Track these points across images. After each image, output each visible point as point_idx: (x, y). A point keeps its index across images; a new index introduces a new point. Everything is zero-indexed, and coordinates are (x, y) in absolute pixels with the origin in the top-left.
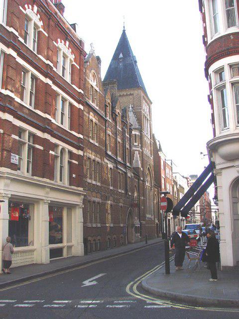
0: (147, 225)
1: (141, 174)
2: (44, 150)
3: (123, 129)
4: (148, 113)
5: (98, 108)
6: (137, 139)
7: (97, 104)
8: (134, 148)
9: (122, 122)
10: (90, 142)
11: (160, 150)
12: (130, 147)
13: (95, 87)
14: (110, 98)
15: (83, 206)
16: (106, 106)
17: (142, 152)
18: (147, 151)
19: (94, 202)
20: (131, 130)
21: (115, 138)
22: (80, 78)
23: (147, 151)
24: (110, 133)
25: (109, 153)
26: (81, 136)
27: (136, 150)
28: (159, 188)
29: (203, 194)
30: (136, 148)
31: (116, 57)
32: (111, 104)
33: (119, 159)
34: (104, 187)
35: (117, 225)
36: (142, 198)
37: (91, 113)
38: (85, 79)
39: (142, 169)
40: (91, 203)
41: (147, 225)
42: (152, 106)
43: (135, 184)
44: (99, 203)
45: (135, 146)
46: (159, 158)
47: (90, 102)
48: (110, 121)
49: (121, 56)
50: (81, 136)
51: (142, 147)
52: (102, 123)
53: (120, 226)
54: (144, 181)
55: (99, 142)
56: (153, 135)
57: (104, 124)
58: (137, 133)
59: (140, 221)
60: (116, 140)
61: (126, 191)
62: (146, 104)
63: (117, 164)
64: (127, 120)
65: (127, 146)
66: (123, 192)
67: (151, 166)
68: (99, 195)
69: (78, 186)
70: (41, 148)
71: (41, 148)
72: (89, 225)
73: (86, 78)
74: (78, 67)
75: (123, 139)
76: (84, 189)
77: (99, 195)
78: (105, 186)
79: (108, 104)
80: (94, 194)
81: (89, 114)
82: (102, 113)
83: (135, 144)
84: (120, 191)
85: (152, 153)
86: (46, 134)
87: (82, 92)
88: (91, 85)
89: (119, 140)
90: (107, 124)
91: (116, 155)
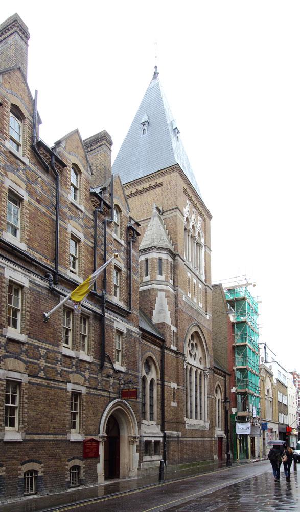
17: (176, 297)
21: (54, 217)
27: (161, 290)
36: (174, 385)
39: (174, 328)
51: (174, 286)
58: (165, 256)
59: (163, 430)
83: (162, 278)
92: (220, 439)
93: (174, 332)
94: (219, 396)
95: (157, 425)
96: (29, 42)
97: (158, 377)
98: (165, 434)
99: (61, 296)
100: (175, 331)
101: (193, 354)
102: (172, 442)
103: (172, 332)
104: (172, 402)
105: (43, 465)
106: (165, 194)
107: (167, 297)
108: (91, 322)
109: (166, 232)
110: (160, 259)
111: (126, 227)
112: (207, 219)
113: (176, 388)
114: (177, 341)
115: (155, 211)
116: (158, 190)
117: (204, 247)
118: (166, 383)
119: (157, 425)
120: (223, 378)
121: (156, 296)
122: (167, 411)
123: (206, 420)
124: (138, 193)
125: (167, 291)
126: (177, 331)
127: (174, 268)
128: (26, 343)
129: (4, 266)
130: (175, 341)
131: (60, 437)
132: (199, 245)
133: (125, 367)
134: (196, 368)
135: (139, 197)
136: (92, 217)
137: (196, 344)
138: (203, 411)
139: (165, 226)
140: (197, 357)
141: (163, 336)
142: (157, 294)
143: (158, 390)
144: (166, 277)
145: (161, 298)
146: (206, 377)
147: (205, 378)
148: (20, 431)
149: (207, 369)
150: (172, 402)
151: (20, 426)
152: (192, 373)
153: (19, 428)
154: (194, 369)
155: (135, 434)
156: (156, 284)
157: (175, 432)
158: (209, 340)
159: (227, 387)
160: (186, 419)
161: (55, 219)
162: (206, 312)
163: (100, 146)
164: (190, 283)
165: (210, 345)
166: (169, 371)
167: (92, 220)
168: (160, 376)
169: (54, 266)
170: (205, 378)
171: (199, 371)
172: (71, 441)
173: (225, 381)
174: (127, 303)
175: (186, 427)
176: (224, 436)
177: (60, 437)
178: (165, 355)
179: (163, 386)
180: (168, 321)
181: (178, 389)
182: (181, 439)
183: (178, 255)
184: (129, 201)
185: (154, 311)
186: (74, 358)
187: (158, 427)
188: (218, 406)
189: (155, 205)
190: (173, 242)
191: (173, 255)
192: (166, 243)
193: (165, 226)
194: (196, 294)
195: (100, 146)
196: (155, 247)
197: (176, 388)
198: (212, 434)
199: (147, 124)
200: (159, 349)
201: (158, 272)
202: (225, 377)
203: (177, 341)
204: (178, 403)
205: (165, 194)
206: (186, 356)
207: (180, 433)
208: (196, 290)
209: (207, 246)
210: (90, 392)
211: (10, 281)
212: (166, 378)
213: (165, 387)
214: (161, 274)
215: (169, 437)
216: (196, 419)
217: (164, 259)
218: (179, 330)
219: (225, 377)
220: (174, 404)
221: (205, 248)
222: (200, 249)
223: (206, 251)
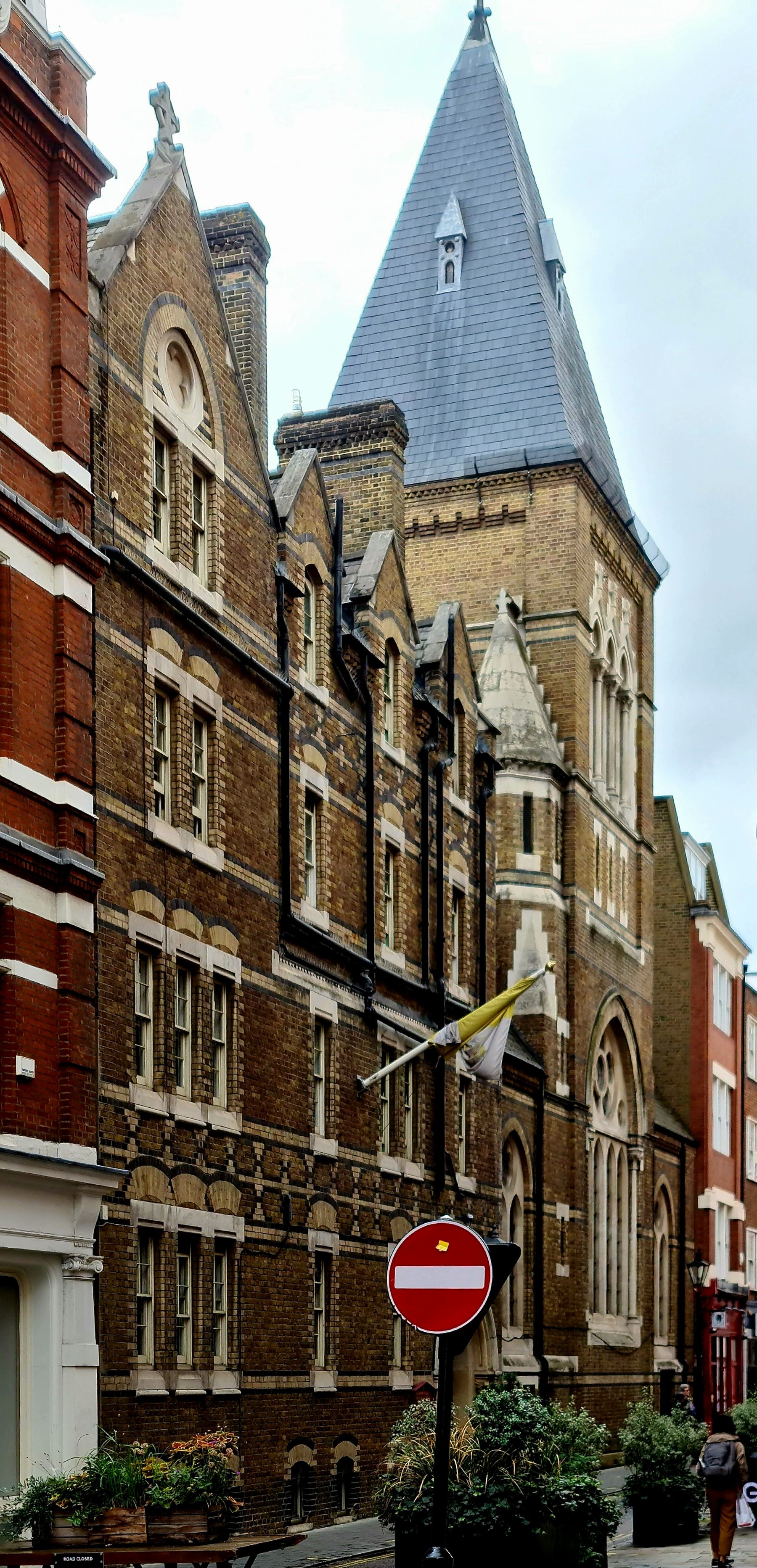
0: (589, 1380)
1: (554, 1062)
2: (62, 990)
3: (422, 757)
4: (624, 648)
5: (215, 601)
6: (539, 825)
7: (212, 576)
8: (519, 893)
9: (419, 708)
10: (159, 844)
11: (714, 903)
12: (480, 879)
13: (189, 438)
14: (324, 534)
15: (98, 1266)
16: (286, 591)
17: (569, 919)
18: (609, 910)
19: (189, 1240)
20: (486, 768)
21: (363, 815)
22: (57, 369)
23: (609, 910)
24: (322, 786)
25: (311, 912)
26: (82, 800)
27: (529, 905)
28: (690, 1154)
29: (281, 878)
30: (527, 886)
31: (414, 243)
32: (324, 573)
33: (392, 958)
34: (269, 1145)
35: (364, 1381)
36: (563, 1211)
37: (161, 637)
38: (104, 376)
39: (563, 1027)
40: (169, 1245)
41: (589, 1380)
42: (663, 602)
43: (513, 1123)
44: (224, 1244)
45: (526, 878)
46: (701, 957)
47: (156, 553)
48: (323, 695)
49: (451, 223)
50: (82, 800)
51: (565, 884)
52: (252, 706)
53: (387, 1389)
54: (574, 1105)
55: (235, 845)
56: (664, 805)
57: (268, 716)
58: (541, 788)
59: (538, 1353)
60: (368, 831)
61: (439, 1162)
62: (614, 585)
63: (367, 996)
64: (459, 694)
65: (457, 873)
66: (415, 1171)
67: (637, 1011)
68: (227, 1194)
69: (59, 1133)
70: (48, 979)
71: (48, 979)
72: (149, 1383)
73: (116, 366)
74: (43, 277)
75: (428, 827)
76: (103, 1157)
77: (227, 1194)
78: (268, 1133)
79: (302, 583)
80: (187, 1184)
81: (144, 640)
82: (254, 639)
83: (529, 862)
84: (388, 1164)
85: (646, 927)
86: (66, 898)
87: (82, 477)
88: (159, 426)
89: (391, 827)
90: (296, 722)
91: (368, 929)
92: (667, 1375)
93: (562, 1037)
94: (662, 1229)
95: (525, 1337)
96: (271, 271)
97: (526, 1190)
98: (544, 1363)
99: (379, 1022)
100: (567, 1035)
101: (602, 1094)
102: (559, 1390)
103: (559, 1040)
104: (558, 1265)
105: (315, 1452)
106: (534, 554)
107: (548, 927)
108: (421, 1070)
109: (536, 691)
110: (528, 799)
111: (413, 671)
112: (645, 591)
113: (567, 1219)
114: (571, 1067)
115: (504, 617)
116: (510, 533)
117: (634, 705)
118: (547, 1208)
119: (525, 1337)
120: (675, 1160)
121: (516, 923)
122: (548, 1293)
123: (633, 1312)
124: (437, 527)
125: (547, 909)
126: (572, 1033)
127: (566, 816)
128: (340, 1160)
129: (307, 986)
130: (565, 1067)
131: (294, 1382)
132: (623, 699)
133: (474, 1180)
134: (610, 1141)
135: (439, 542)
136: (415, 769)
137: (609, 1056)
138: (624, 1284)
139: (535, 668)
140: (610, 1102)
141: (541, 1061)
142: (518, 919)
143: (527, 1229)
144: (545, 860)
145: (531, 930)
146: (635, 1166)
147: (630, 1171)
148: (328, 1367)
149: (640, 1140)
150: (558, 1265)
151: (330, 1357)
152: (600, 1162)
153: (326, 1361)
154: (605, 1144)
155: (492, 1369)
156: (516, 883)
157: (564, 1359)
158: (644, 1038)
159: (689, 1192)
160: (588, 1316)
161: (365, 819)
162: (639, 937)
163: (375, 453)
164: (601, 853)
165: (648, 1054)
166: (553, 1169)
167: (417, 779)
168: (531, 1186)
169: (365, 947)
170: (630, 1171)
171: (617, 1148)
172: (316, 1390)
173: (682, 1169)
174: (475, 986)
175: (590, 1342)
176: (678, 1367)
177: (294, 1382)
178: (545, 1119)
179: (539, 1214)
180: (552, 1009)
181: (572, 1220)
182: (579, 1380)
183: (577, 778)
184: (412, 549)
185: (510, 972)
186: (396, 1177)
187: (528, 1343)
188: (661, 1259)
189: (503, 593)
190: (560, 731)
191: (562, 778)
192: (554, 752)
193: (535, 668)
194: (614, 887)
195: (375, 453)
196: (514, 760)
197: (567, 1219)
198: (649, 1358)
199: (459, 246)
200: (529, 1102)
201: (519, 842)
202: (682, 1156)
203: (571, 1067)
204: (572, 1268)
205: (534, 554)
206: (590, 1111)
207: (575, 1360)
208: (614, 872)
209: (646, 699)
210: (364, 1250)
211: (318, 1018)
212: (547, 1190)
213: (545, 1218)
214: (528, 848)
215: (555, 1374)
216: (608, 1311)
217: (540, 799)
218: (577, 1030)
219: (682, 1156)
220: (563, 1271)
221: (640, 706)
222: (622, 713)
223: (640, 717)
